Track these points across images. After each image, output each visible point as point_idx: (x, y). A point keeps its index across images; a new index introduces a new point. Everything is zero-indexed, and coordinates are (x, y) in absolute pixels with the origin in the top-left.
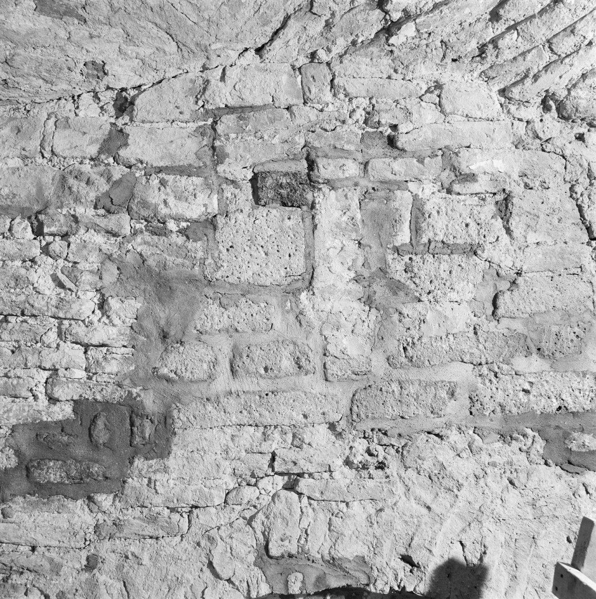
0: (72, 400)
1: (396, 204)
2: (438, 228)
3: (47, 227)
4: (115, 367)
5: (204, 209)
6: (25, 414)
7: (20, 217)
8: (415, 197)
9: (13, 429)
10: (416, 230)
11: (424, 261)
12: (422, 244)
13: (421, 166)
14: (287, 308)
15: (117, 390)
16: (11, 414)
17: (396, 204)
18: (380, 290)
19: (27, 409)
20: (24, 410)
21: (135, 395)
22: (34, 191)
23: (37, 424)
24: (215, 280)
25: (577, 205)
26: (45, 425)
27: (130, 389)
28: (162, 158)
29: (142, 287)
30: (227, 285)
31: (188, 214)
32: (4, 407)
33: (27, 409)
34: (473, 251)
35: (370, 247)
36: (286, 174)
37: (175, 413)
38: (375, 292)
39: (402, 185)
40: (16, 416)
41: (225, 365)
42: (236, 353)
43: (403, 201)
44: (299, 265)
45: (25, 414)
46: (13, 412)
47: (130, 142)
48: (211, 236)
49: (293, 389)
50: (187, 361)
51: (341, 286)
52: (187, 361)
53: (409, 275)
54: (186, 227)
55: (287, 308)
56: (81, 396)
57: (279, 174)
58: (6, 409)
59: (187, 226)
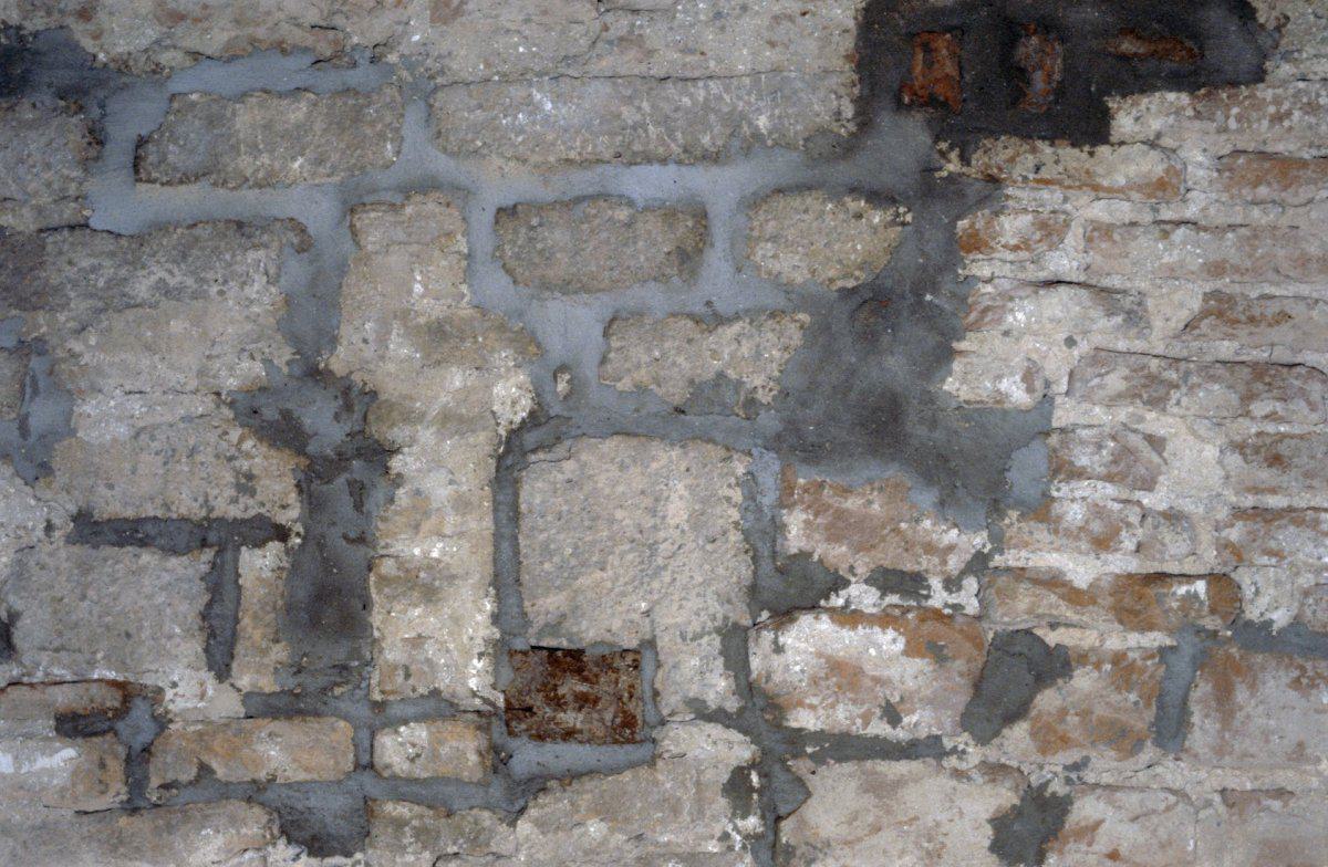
0: (1112, 145)
1: (280, 653)
2: (164, 587)
3: (1196, 596)
4: (1007, 226)
5: (781, 640)
6: (1235, 111)
7: (1275, 627)
8: (222, 672)
9: (1259, 76)
10: (221, 586)
11: (206, 501)
12: (211, 546)
13: (205, 758)
14: (567, 377)
15: (1000, 169)
16: (1272, 109)
17: (280, 653)
18: (325, 424)
19: (1233, 124)
20: (1239, 119)
21: (954, 155)
22: (1241, 694)
23: (1204, 85)
24: (754, 451)
25: (153, 716)
26: (1177, 81)
27: (964, 169)
28: (900, 783)
29: (938, 435)
30: (719, 437)
31: (825, 624)
32: (1290, 128)
33: (1233, 124)
34: (90, 529)
35: (345, 537)
36: (569, 734)
37: (849, 111)
38: (337, 417)
39: (264, 708)
40: (1259, 105)
41: (720, 233)
42: (688, 258)
43: (257, 673)
44: (537, 490)
45: (1235, 111)
46: (1274, 116)
47: (989, 831)
48: (766, 567)
49: (551, 169)
50: (844, 241)
51: (427, 435)
52: (844, 241)
53: (245, 465)
54: (833, 597)
55: (567, 377)
56: (1091, 154)
57: (586, 736)
58: (1286, 123)
59: (827, 598)
